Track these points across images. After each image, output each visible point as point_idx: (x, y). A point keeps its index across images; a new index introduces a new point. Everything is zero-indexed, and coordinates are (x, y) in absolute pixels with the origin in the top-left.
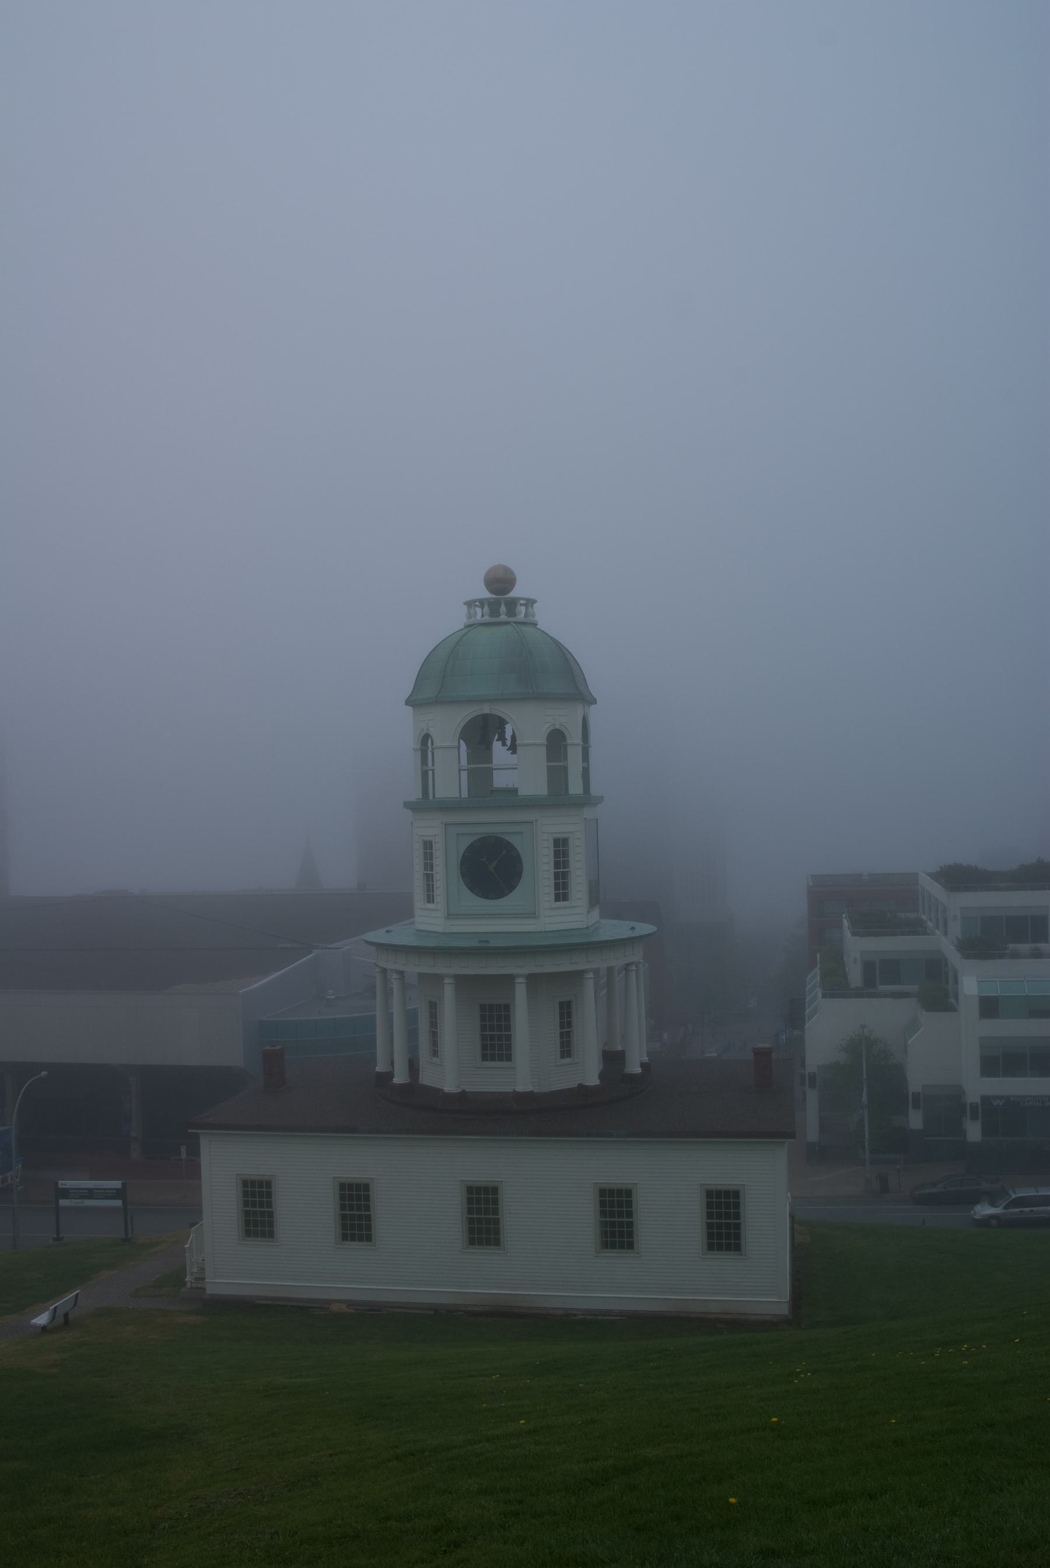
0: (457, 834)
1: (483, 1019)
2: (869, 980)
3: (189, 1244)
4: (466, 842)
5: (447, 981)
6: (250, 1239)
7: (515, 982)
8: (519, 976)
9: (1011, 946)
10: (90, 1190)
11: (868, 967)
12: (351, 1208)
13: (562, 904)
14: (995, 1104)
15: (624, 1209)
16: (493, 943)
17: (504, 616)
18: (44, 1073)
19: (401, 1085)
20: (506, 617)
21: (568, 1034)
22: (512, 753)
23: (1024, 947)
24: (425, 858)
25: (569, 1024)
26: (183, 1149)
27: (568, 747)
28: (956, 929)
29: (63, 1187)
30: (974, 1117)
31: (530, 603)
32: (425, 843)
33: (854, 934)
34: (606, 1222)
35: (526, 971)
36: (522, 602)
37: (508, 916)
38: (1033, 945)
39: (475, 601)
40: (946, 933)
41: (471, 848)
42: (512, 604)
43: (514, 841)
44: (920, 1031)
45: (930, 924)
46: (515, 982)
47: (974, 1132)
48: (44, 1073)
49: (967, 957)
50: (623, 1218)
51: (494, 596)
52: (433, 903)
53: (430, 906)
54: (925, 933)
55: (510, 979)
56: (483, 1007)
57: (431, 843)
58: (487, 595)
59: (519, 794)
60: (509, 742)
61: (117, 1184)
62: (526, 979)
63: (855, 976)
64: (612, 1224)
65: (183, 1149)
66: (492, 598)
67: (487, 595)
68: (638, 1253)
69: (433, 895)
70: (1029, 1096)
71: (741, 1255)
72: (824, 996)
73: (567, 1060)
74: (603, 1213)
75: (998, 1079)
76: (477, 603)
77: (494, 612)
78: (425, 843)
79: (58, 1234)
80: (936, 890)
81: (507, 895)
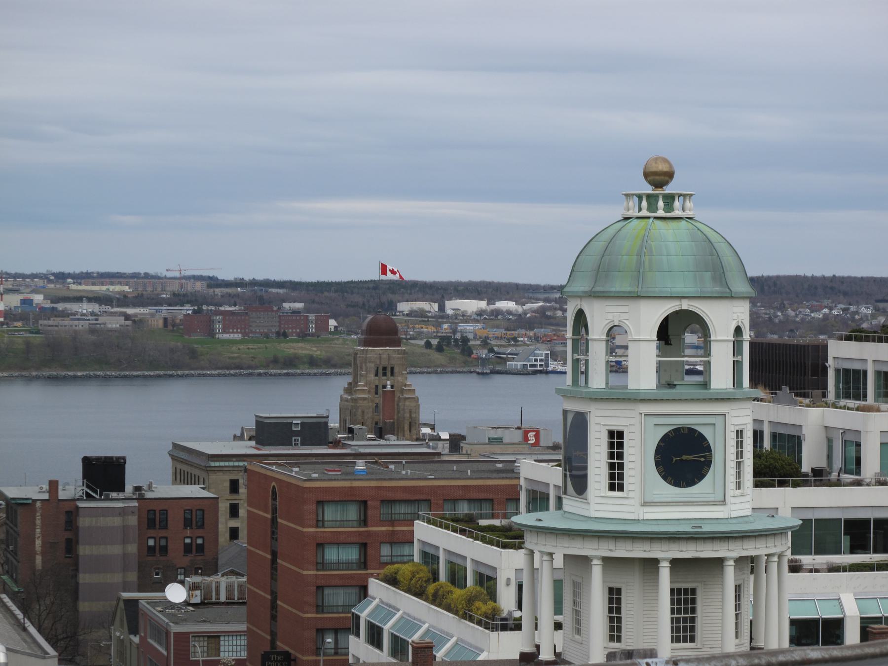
4: (662, 432)
5: (595, 562)
7: (592, 563)
8: (664, 559)
16: (707, 528)
17: (662, 211)
20: (648, 213)
27: (712, 342)
35: (736, 554)
37: (700, 503)
41: (665, 439)
43: (706, 432)
46: (592, 563)
58: (649, 190)
62: (734, 563)
77: (652, 207)
78: (611, 434)
81: (697, 483)
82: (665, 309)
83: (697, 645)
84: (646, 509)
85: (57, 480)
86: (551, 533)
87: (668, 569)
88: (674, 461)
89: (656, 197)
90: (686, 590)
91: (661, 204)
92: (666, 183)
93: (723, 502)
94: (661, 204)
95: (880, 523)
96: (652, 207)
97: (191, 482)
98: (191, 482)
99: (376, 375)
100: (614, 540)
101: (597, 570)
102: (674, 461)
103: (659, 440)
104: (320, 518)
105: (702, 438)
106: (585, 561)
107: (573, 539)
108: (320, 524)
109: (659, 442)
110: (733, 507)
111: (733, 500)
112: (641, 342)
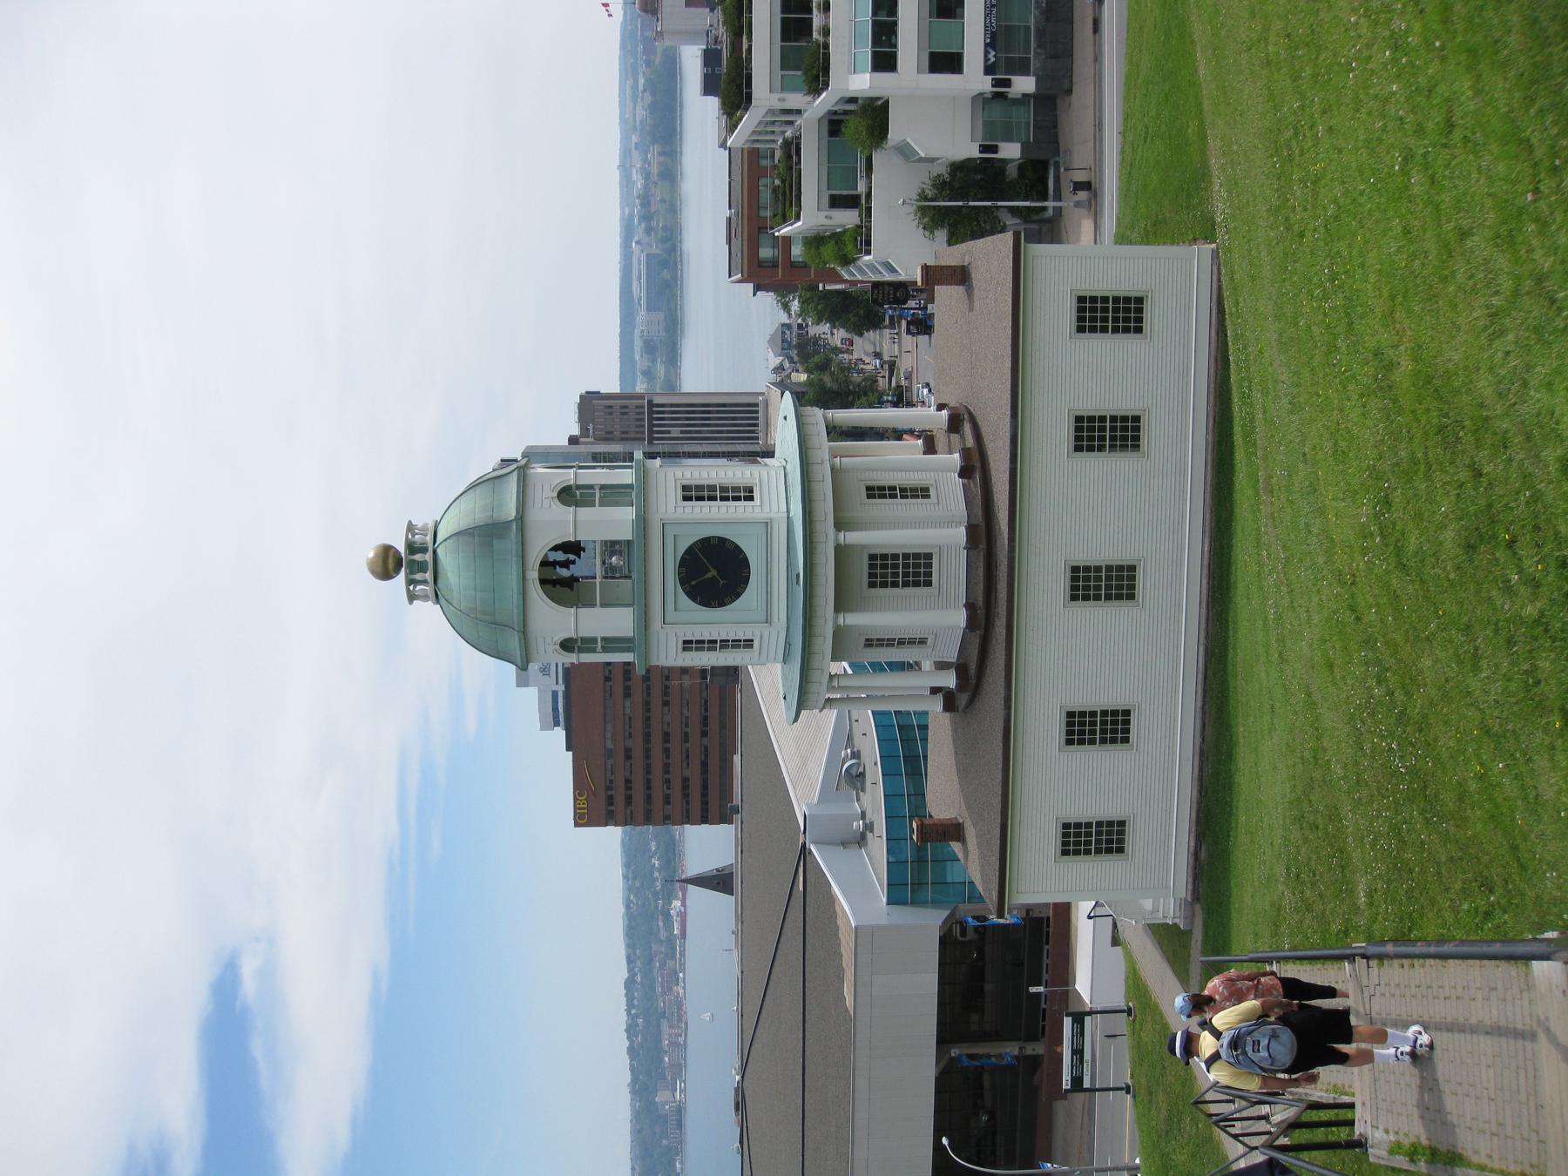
0: (675, 610)
1: (884, 585)
2: (850, 202)
3: (1131, 919)
5: (841, 621)
6: (1126, 840)
8: (836, 538)
9: (815, 35)
10: (1074, 1052)
11: (837, 202)
12: (1093, 732)
13: (756, 494)
14: (993, 59)
15: (1087, 324)
18: (945, 1141)
19: (958, 677)
21: (903, 490)
22: (584, 551)
23: (817, 20)
24: (702, 649)
25: (893, 488)
26: (1033, 990)
28: (796, 100)
29: (1069, 1083)
30: (1007, 83)
31: (411, 527)
32: (685, 649)
33: (798, 218)
34: (1111, 446)
36: (410, 536)
38: (815, 11)
39: (408, 590)
40: (799, 112)
41: (693, 594)
42: (412, 548)
43: (683, 546)
44: (910, 142)
45: (789, 134)
47: (1024, 84)
48: (945, 1141)
49: (826, 85)
50: (1106, 435)
51: (403, 569)
52: (752, 641)
53: (756, 644)
54: (799, 138)
55: (839, 549)
56: (872, 585)
57: (685, 642)
58: (401, 577)
59: (631, 538)
60: (572, 557)
61: (1067, 1022)
63: (847, 218)
64: (1113, 438)
65: (1033, 990)
66: (406, 571)
67: (401, 577)
68: (1145, 410)
69: (745, 641)
70: (985, 21)
71: (1147, 297)
72: (868, 252)
73: (932, 492)
74: (1101, 448)
75: (965, 55)
76: (411, 588)
77: (422, 567)
78: (685, 649)
79: (1121, 1089)
80: (749, 121)
82: (536, 593)
83: (932, 485)
84: (775, 619)
85: (687, 9)
86: (808, 664)
87: (847, 533)
88: (725, 582)
89: (411, 563)
90: (871, 566)
91: (418, 557)
92: (397, 551)
93: (767, 525)
94: (418, 557)
95: (786, 7)
96: (422, 567)
97: (705, 804)
98: (705, 804)
99: (567, 645)
100: (813, 656)
101: (851, 619)
102: (725, 582)
103: (691, 601)
104: (771, 264)
105: (690, 551)
106: (839, 633)
107: (815, 611)
108: (775, 264)
109: (696, 603)
110: (775, 509)
111: (766, 509)
112: (578, 519)
